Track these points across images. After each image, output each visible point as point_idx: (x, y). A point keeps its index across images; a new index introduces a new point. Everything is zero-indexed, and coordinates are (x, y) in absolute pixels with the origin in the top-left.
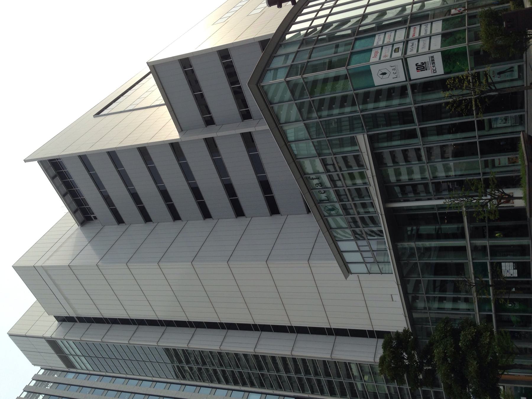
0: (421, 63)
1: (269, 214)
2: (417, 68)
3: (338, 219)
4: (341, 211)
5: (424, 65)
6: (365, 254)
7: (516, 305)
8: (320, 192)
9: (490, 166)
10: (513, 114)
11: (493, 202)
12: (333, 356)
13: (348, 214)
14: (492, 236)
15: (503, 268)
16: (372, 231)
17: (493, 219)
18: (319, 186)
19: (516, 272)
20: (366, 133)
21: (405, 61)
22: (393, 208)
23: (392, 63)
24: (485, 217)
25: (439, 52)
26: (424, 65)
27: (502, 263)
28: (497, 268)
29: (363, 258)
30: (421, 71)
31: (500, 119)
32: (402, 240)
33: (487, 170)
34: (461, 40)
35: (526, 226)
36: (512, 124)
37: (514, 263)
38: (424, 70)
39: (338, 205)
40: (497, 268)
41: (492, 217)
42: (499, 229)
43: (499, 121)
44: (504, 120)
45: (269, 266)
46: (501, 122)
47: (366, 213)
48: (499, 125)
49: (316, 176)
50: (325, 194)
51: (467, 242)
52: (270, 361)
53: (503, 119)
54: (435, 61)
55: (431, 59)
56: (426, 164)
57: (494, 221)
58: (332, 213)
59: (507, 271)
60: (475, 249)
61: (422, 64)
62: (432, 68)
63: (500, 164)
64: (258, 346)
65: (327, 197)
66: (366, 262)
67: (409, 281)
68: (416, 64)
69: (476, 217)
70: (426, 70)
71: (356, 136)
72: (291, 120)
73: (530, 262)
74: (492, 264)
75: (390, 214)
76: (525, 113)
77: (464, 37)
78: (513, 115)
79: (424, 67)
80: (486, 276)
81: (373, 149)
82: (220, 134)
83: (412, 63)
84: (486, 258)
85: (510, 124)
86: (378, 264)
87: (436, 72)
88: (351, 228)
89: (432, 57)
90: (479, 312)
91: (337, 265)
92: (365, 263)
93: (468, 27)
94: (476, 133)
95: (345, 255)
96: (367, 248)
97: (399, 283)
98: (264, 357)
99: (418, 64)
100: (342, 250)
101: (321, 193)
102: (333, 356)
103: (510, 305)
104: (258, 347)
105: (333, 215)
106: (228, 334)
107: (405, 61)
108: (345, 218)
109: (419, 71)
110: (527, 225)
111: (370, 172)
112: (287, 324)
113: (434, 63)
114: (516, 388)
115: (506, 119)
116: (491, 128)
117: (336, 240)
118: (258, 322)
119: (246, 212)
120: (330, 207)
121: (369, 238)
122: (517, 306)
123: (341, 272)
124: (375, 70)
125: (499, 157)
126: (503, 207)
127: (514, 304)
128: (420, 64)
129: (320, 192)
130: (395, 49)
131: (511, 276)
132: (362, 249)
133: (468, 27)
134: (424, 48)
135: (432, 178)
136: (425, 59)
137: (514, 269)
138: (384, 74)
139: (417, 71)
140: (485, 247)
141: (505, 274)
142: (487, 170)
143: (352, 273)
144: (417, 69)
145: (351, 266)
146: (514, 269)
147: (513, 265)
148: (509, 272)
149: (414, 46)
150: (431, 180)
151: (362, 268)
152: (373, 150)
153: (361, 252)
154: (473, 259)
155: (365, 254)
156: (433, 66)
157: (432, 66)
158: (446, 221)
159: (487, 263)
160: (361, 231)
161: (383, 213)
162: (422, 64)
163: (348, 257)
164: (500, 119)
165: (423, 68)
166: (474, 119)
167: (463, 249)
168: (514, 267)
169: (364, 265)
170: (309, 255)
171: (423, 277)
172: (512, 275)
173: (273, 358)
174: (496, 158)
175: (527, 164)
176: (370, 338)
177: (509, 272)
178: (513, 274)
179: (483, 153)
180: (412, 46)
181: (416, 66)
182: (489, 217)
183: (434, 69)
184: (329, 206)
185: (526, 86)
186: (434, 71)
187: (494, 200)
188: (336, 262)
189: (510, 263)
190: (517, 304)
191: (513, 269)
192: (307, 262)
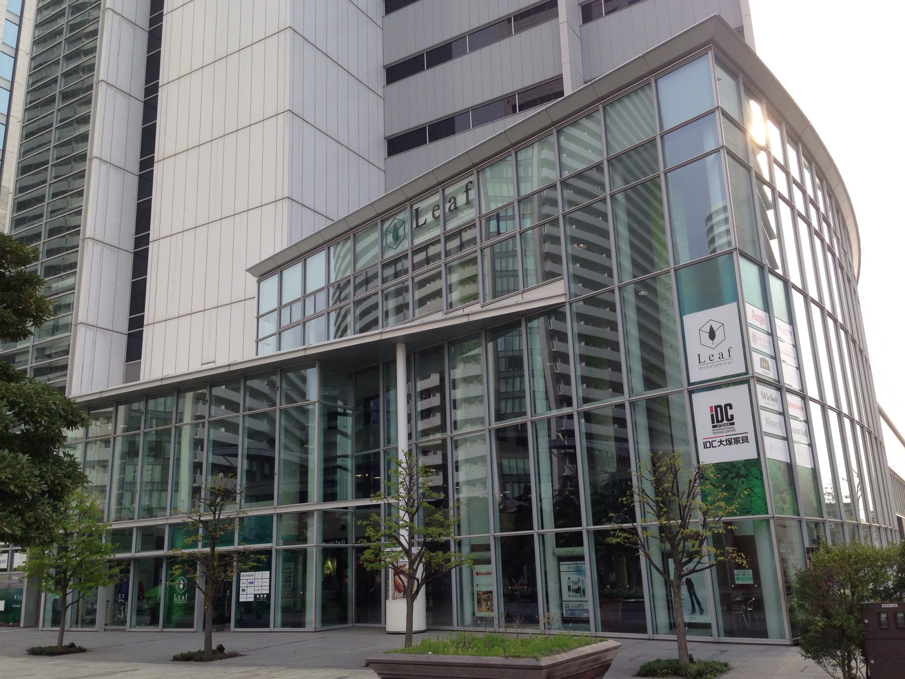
0: (732, 416)
1: (388, 134)
2: (720, 406)
3: (376, 250)
4: (390, 254)
5: (725, 422)
6: (297, 308)
7: (181, 597)
8: (437, 208)
9: (476, 555)
10: (590, 605)
11: (402, 558)
12: (90, 243)
13: (385, 266)
14: (327, 554)
15: (258, 574)
16: (345, 316)
17: (363, 558)
18: (449, 204)
19: (338, 450)
20: (568, 300)
21: (745, 379)
22: (394, 362)
23: (738, 352)
24: (369, 539)
25: (759, 455)
26: (725, 422)
27: (269, 572)
28: (253, 561)
29: (290, 304)
30: (712, 415)
31: (579, 579)
32: (325, 382)
33: (466, 549)
34: (781, 503)
35: (343, 619)
36: (567, 603)
37: (269, 595)
38: (713, 422)
39: (405, 245)
40: (261, 562)
41: (367, 554)
42: (342, 566)
43: (575, 577)
44: (576, 587)
45: (281, 117)
46: (571, 581)
47: (386, 314)
48: (564, 577)
49: (473, 200)
50: (432, 219)
51: (315, 504)
52: (82, 112)
53: (580, 584)
54: (734, 446)
55: (740, 436)
56: (488, 427)
57: (358, 558)
58: (388, 238)
59: (252, 581)
60: (302, 518)
61: (730, 418)
62: (718, 439)
63: (478, 574)
64: (111, 91)
65: (425, 223)
66: (282, 311)
67: (237, 390)
68: (730, 406)
69: (371, 521)
70: (714, 427)
71: (562, 279)
72: (548, 224)
73: (269, 627)
74: (268, 552)
75: (386, 349)
76: (592, 632)
77: (785, 510)
78: (590, 606)
79: (722, 420)
80: (244, 540)
81: (530, 315)
82: (564, 29)
83: (736, 396)
84: (281, 542)
85: (565, 596)
86: (278, 334)
87: (705, 447)
88: (355, 278)
89: (745, 440)
90: (170, 525)
91: (278, 250)
92: (280, 307)
93: (804, 521)
94: (550, 529)
95: (297, 269)
96: (310, 312)
97: (233, 368)
98: (88, 102)
99: (731, 408)
100: (307, 260)
101: (434, 211)
102: (90, 243)
103: (181, 586)
104: (108, 88)
105: (385, 240)
106: (139, 31)
107: (745, 379)
108: (377, 264)
109: (711, 411)
110: (346, 622)
111: (477, 312)
112: (158, 154)
113: (731, 443)
114: (20, 592)
115: (580, 591)
116: (561, 559)
117: (329, 248)
118: (162, 94)
119: (396, 85)
120: (401, 232)
121: (333, 316)
122: (179, 600)
123: (263, 259)
124: (724, 314)
125: (494, 574)
126: (387, 578)
127: (184, 594)
128: (730, 412)
129: (437, 208)
130: (768, 362)
131: (241, 589)
132: (310, 302)
133: (804, 521)
134: (767, 422)
135: (455, 438)
136: (743, 424)
137: (255, 595)
138: (712, 335)
139: (711, 408)
140: (305, 540)
141: (246, 577)
142: (466, 549)
143: (259, 282)
144: (716, 407)
145: (274, 279)
146: (255, 595)
147: (263, 594)
148: (249, 585)
149: (771, 402)
150: (452, 438)
151: (269, 302)
152: (526, 318)
153: (302, 299)
154: (280, 516)
155: (298, 308)
156: (721, 441)
157: (724, 439)
158: (360, 476)
159: (271, 542)
160: (346, 298)
161: (385, 337)
162: (730, 418)
163: (293, 275)
164: (579, 579)
165: (720, 419)
166: (587, 526)
167: (303, 497)
168: (260, 595)
169: (275, 305)
170: (300, 202)
171: (244, 416)
172: (244, 590)
173: (85, 120)
174: (492, 568)
175: (543, 664)
176: (130, 319)
177: (249, 585)
178: (245, 593)
179: (505, 544)
180: (772, 398)
181: (726, 405)
182: (703, 529)
183: (715, 444)
184: (406, 229)
185: (687, 639)
186: (708, 444)
187: (406, 559)
188: (285, 247)
189: (268, 588)
190: (183, 598)
191: (256, 593)
192: (286, 195)
